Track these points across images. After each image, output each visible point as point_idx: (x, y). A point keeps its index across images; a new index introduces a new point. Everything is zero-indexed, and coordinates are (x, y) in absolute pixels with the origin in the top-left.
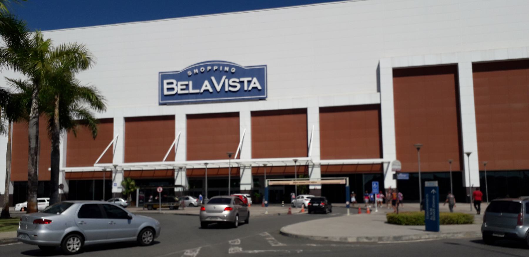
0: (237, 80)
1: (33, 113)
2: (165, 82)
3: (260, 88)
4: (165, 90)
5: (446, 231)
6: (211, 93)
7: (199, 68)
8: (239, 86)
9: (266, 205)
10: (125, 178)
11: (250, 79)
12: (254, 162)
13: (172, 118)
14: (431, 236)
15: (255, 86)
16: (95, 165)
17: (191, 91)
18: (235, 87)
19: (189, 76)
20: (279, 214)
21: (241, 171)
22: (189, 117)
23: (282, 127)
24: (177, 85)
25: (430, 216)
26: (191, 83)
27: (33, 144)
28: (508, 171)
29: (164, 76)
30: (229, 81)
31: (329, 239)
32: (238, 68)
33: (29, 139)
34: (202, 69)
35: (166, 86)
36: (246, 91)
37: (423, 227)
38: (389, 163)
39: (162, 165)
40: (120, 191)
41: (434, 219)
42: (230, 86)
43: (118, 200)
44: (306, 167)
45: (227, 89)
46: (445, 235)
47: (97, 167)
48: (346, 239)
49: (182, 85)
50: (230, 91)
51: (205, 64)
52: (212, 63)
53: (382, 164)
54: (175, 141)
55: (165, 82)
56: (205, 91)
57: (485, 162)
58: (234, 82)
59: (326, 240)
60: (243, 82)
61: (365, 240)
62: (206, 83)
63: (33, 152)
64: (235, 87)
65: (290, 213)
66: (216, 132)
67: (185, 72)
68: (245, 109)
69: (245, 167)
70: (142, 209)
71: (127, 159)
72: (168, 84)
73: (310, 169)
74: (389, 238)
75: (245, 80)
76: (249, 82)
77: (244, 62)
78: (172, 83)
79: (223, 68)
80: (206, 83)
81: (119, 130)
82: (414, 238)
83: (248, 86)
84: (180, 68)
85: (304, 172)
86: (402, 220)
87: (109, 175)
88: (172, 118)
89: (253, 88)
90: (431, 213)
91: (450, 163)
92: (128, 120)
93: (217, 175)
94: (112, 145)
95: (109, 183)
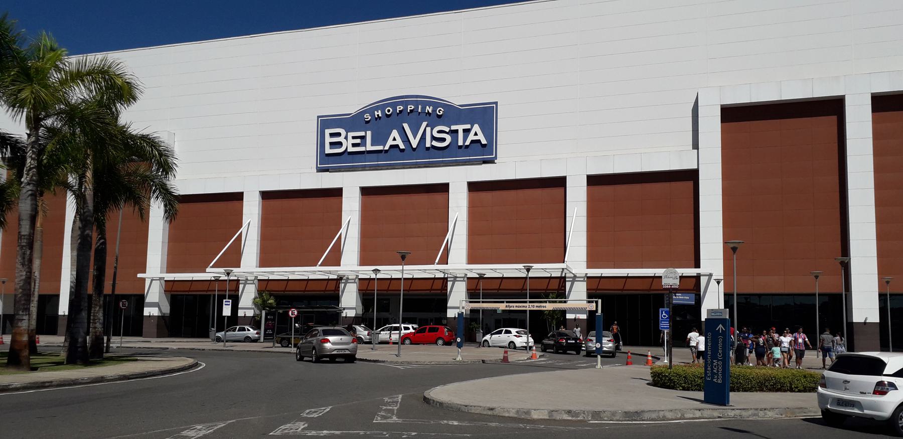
0: (447, 129)
1: (28, 174)
2: (328, 132)
3: (484, 142)
4: (327, 146)
5: (744, 404)
6: (402, 150)
7: (382, 108)
8: (449, 138)
9: (459, 346)
10: (260, 292)
11: (468, 126)
12: (471, 270)
13: (337, 193)
14: (712, 412)
15: (476, 138)
16: (208, 270)
17: (369, 147)
18: (444, 140)
19: (367, 122)
20: (483, 361)
21: (450, 284)
22: (366, 191)
23: (522, 209)
24: (346, 138)
25: (713, 374)
26: (369, 133)
27: (25, 230)
28: (760, 296)
29: (325, 123)
30: (432, 130)
31: (495, 413)
32: (448, 107)
33: (20, 219)
34: (389, 110)
35: (328, 140)
36: (460, 147)
37: (701, 395)
38: (710, 275)
39: (317, 272)
40: (250, 313)
41: (720, 381)
42: (434, 138)
43: (244, 330)
44: (562, 280)
45: (428, 145)
46: (738, 412)
47: (211, 273)
48: (528, 412)
49: (354, 138)
50: (433, 147)
51: (393, 102)
52: (404, 100)
53: (698, 278)
54: (343, 231)
55: (328, 132)
56: (392, 146)
57: (888, 278)
58: (439, 132)
59: (490, 413)
60: (456, 131)
61: (566, 417)
62: (395, 133)
63: (24, 242)
64: (444, 140)
65: (505, 359)
66: (408, 218)
67: (361, 114)
68: (458, 178)
69: (455, 278)
70: (271, 344)
71: (265, 261)
72: (332, 135)
73: (568, 285)
74: (614, 414)
75: (460, 128)
76: (467, 132)
77: (459, 98)
78: (339, 134)
79: (424, 108)
80: (395, 133)
81: (252, 212)
82: (669, 415)
83: (465, 140)
84: (352, 108)
85: (557, 288)
86: (676, 379)
87: (440, 287)
88: (337, 193)
89: (473, 142)
90: (715, 371)
91: (817, 277)
92: (266, 195)
93: (305, 291)
94: (340, 237)
95: (335, 298)
